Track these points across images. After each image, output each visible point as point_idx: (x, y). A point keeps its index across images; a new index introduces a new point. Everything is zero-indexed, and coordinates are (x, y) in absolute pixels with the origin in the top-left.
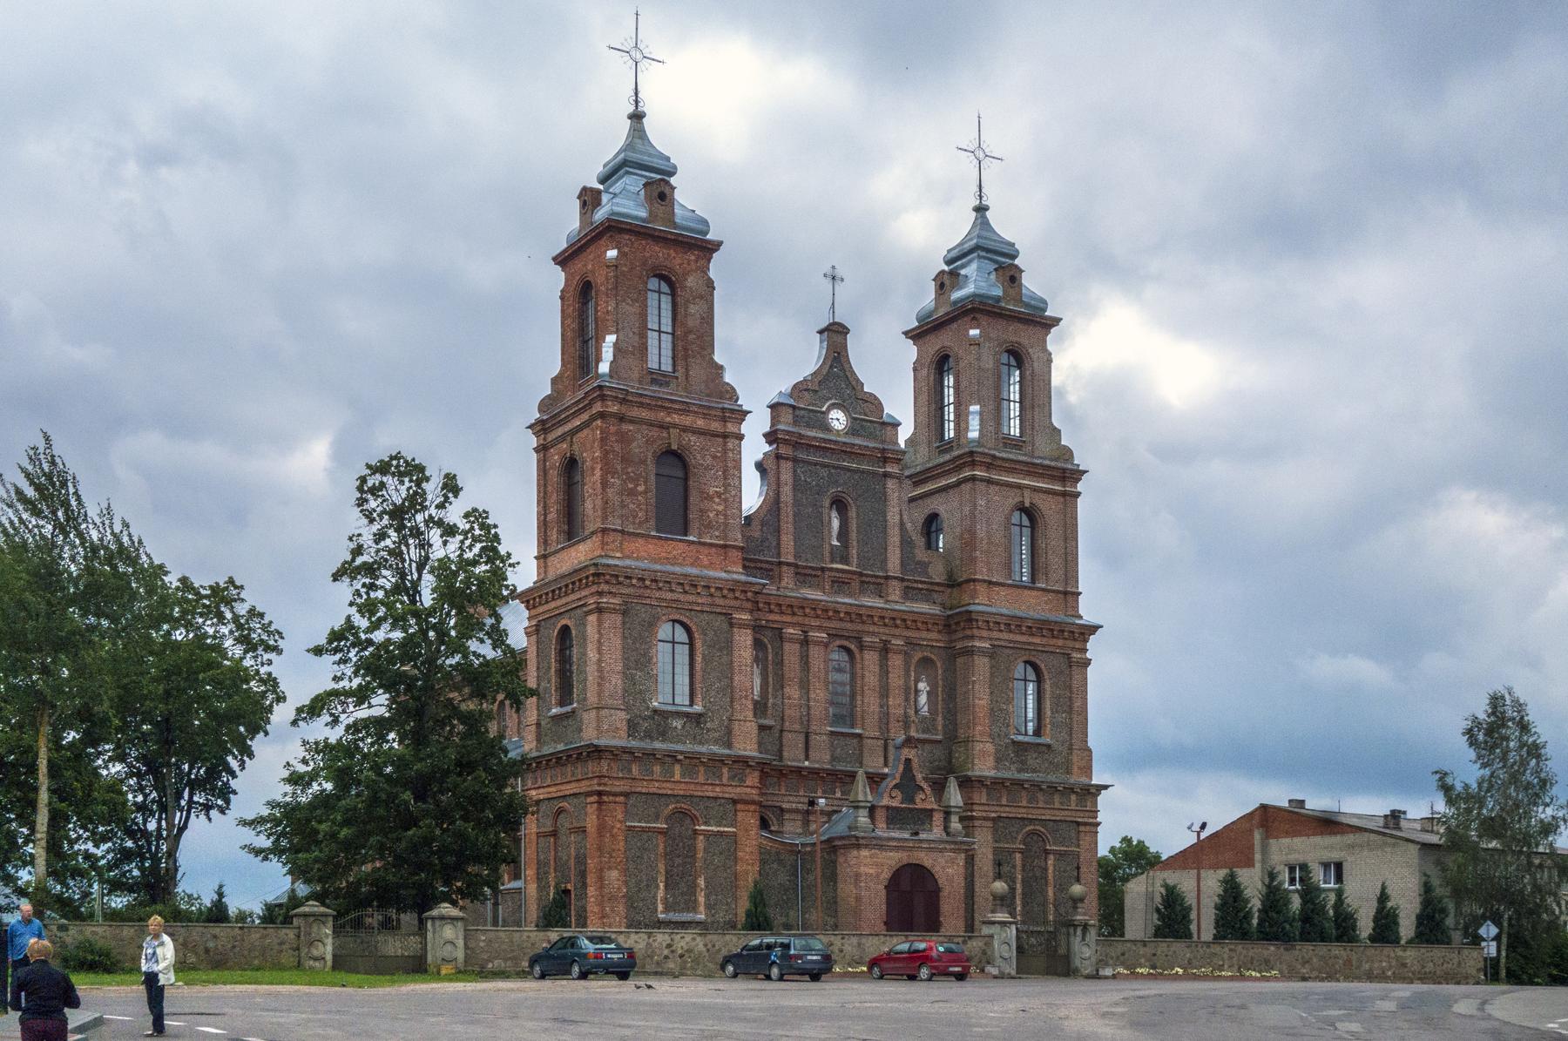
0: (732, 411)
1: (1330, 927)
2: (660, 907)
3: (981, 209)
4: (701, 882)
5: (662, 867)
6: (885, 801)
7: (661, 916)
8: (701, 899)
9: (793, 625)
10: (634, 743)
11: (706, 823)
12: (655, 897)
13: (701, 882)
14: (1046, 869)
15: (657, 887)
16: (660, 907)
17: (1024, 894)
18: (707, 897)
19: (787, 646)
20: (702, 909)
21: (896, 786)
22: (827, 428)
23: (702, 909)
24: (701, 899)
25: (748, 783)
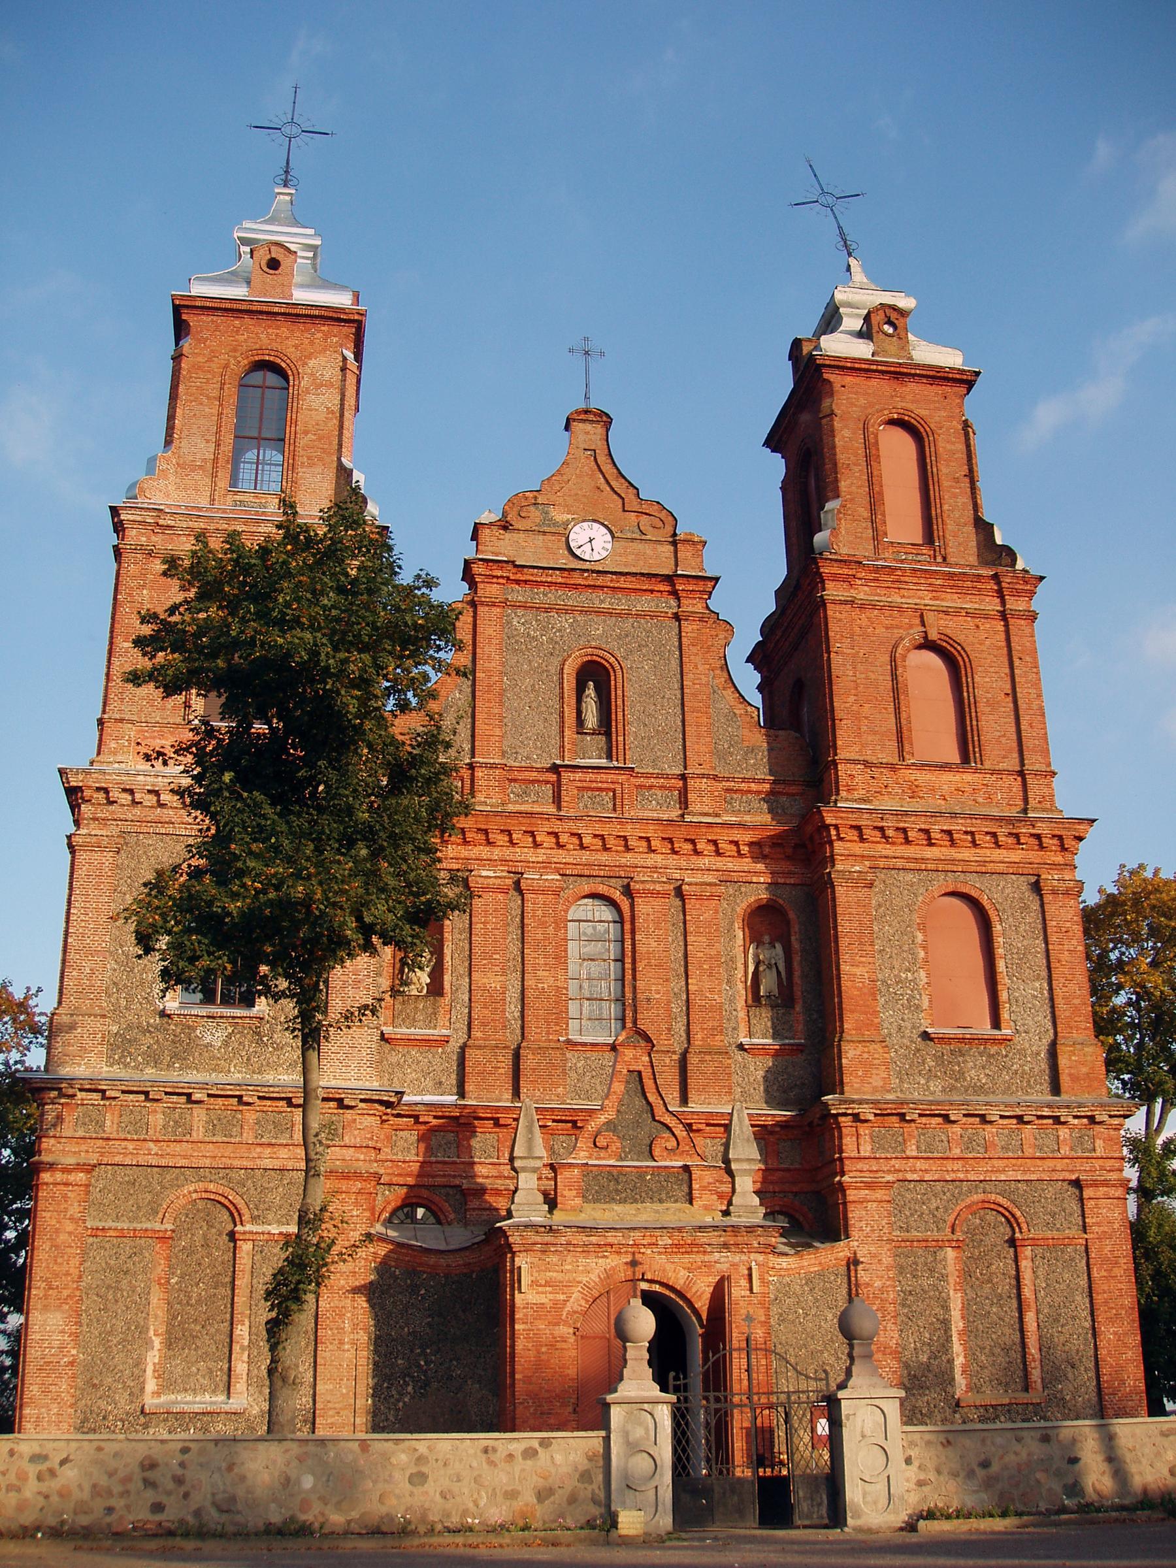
12: (139, 1363)
15: (148, 1344)
21: (610, 1126)
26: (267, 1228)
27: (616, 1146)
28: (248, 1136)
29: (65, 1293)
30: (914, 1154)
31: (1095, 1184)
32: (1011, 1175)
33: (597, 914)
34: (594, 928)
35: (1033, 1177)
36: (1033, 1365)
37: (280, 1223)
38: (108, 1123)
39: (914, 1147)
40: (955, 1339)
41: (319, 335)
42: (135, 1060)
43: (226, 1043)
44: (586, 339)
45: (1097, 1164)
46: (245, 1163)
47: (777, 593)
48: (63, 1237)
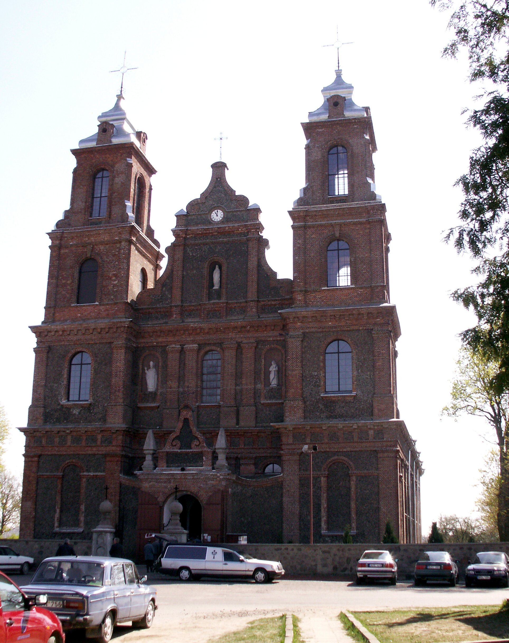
0: (373, 208)
1: (383, 534)
2: (56, 524)
3: (120, 97)
4: (83, 507)
5: (58, 498)
6: (168, 448)
7: (57, 530)
8: (82, 519)
9: (175, 343)
10: (48, 427)
11: (88, 471)
12: (53, 517)
13: (83, 507)
14: (349, 488)
15: (55, 511)
16: (56, 524)
17: (329, 507)
18: (85, 517)
19: (170, 355)
20: (82, 524)
21: (177, 438)
22: (210, 222)
23: (82, 524)
24: (82, 519)
25: (114, 443)
26: (90, 474)
27: (179, 445)
28: (84, 444)
29: (32, 495)
30: (309, 442)
31: (383, 452)
32: (349, 449)
33: (213, 357)
34: (212, 362)
35: (358, 450)
36: (353, 521)
37: (94, 472)
38: (43, 441)
39: (309, 440)
40: (322, 510)
41: (119, 154)
42: (53, 420)
43: (79, 413)
44: (221, 133)
45: (385, 444)
46: (84, 453)
47: (153, 231)
48: (31, 478)
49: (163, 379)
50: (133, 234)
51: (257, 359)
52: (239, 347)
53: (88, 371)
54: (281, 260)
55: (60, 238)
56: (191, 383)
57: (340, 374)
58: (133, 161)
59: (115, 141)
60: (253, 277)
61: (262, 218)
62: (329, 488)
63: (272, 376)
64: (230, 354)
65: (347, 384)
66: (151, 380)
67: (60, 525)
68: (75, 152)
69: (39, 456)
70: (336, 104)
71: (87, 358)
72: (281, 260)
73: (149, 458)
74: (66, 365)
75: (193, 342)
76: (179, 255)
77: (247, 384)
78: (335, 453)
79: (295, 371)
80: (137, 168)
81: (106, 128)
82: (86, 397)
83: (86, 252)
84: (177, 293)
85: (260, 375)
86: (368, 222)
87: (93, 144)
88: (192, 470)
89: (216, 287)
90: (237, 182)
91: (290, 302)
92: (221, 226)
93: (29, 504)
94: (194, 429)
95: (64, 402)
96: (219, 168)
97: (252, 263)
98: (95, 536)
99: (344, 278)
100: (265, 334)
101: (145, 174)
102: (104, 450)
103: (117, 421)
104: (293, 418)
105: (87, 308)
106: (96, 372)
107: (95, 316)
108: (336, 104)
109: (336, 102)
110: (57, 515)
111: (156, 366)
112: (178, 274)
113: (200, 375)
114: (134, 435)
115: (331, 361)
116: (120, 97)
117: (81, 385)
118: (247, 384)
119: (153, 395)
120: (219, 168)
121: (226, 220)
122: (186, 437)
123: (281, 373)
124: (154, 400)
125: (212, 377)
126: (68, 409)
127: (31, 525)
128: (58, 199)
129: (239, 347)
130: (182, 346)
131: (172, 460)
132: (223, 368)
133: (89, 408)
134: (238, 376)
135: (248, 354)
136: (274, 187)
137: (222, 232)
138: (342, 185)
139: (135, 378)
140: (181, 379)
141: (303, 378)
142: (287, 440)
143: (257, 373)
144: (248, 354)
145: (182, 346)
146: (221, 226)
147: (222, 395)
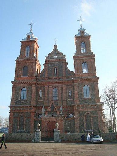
3: (31, 30)
6: (48, 110)
49: (44, 94)
50: (34, 61)
51: (66, 90)
52: (62, 87)
53: (26, 92)
54: (71, 67)
55: (18, 62)
56: (51, 95)
57: (86, 93)
58: (35, 44)
59: (31, 40)
60: (64, 71)
61: (66, 58)
62: (86, 119)
63: (70, 93)
64: (60, 88)
65: (89, 95)
66: (41, 95)
67: (19, 130)
68: (21, 42)
69: (13, 113)
70: (82, 33)
71: (25, 89)
72: (71, 67)
73: (43, 113)
74: (20, 91)
75: (51, 86)
76: (47, 65)
77: (64, 95)
78: (87, 111)
79: (76, 92)
80: (36, 46)
81: (28, 36)
82: (25, 98)
83: (25, 63)
84: (46, 74)
85: (67, 93)
86: (91, 59)
87: (26, 40)
88: (54, 116)
89: (56, 73)
90: (60, 49)
91: (74, 76)
92: (56, 60)
93: (11, 125)
94: (54, 106)
95: (20, 100)
96: (55, 46)
97: (64, 68)
98: (36, 132)
99: (84, 71)
100: (68, 84)
101: (37, 48)
102: (31, 111)
103: (33, 104)
104: (77, 103)
105: (25, 77)
106: (28, 92)
107: (25, 79)
108: (82, 33)
109: (82, 32)
110: (18, 127)
111: (42, 91)
112: (47, 70)
113: (52, 93)
114: (38, 108)
115: (84, 90)
116: (31, 30)
117: (24, 96)
118: (64, 95)
119: (41, 98)
120: (55, 46)
121: (57, 58)
122: (52, 108)
123: (73, 93)
124: (42, 99)
125: (56, 94)
126: (21, 101)
127: (12, 130)
128: (17, 53)
129: (62, 87)
130: (48, 87)
131: (49, 113)
132: (58, 91)
133: (26, 101)
134: (62, 93)
135: (64, 88)
136: (69, 51)
137: (57, 61)
138: (83, 51)
139: (37, 94)
140: (48, 94)
141: (78, 94)
142: (75, 108)
143: (66, 93)
144: (64, 88)
145: (48, 87)
146: (56, 60)
147: (58, 98)
